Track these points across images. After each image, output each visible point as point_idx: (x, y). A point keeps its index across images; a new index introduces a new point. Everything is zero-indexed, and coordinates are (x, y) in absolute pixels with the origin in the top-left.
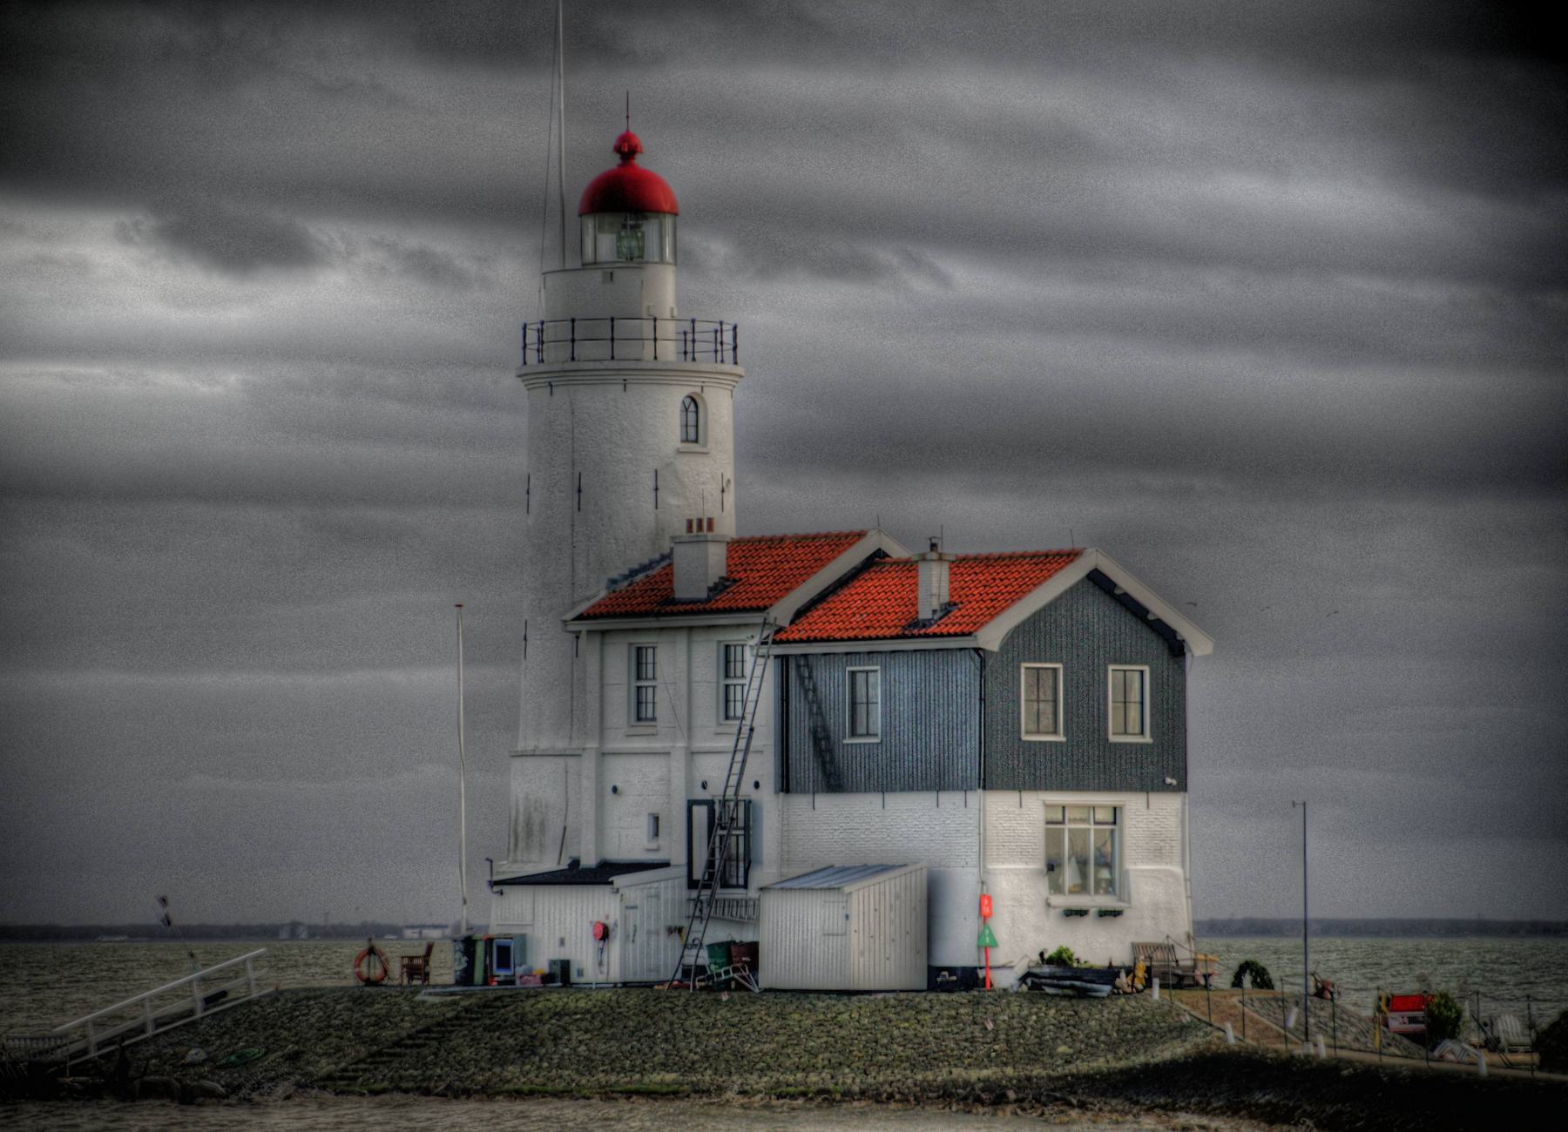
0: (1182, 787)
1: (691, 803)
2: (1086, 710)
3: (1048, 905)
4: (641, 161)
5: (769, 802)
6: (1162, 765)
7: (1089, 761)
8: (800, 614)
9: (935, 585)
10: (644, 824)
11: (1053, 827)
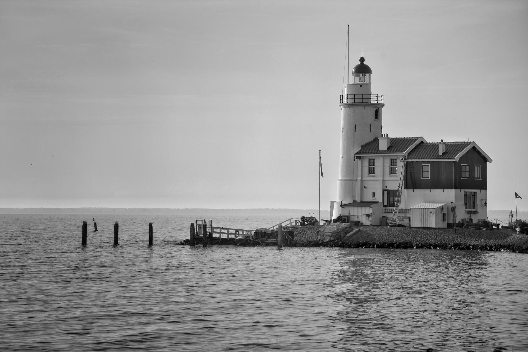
1: (384, 191)
4: (365, 63)
8: (410, 153)
11: (466, 194)
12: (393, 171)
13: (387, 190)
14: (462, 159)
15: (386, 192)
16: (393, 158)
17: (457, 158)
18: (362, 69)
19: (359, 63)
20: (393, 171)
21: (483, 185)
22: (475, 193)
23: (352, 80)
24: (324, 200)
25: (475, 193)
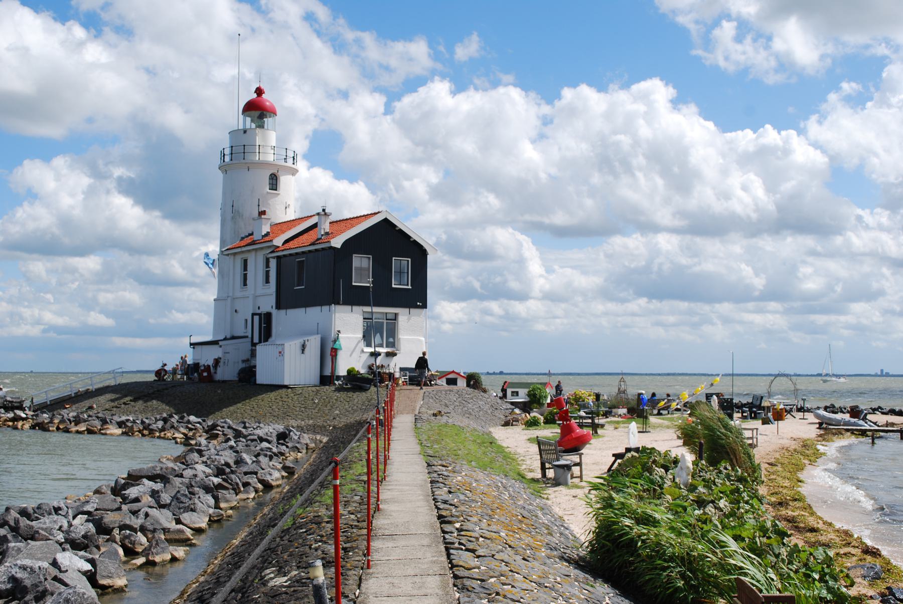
1: (253, 315)
3: (363, 351)
5: (274, 312)
7: (382, 294)
9: (326, 227)
10: (243, 322)
12: (267, 281)
13: (260, 315)
14: (347, 243)
15: (256, 318)
16: (244, 256)
17: (337, 242)
18: (257, 109)
19: (255, 96)
21: (416, 298)
22: (396, 315)
23: (236, 119)
25: (396, 315)
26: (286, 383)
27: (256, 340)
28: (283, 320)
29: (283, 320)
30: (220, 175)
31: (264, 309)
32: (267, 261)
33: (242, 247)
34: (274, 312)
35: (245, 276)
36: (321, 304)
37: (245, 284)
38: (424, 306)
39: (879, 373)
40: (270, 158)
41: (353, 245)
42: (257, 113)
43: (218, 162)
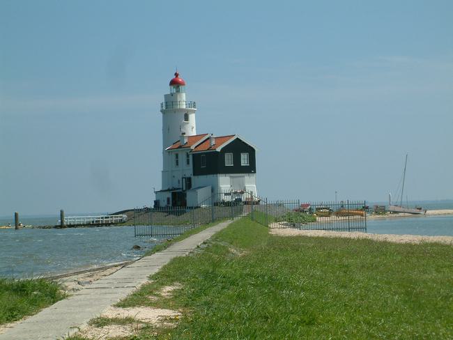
0: (255, 172)
1: (183, 178)
2: (237, 160)
5: (192, 176)
6: (251, 169)
7: (237, 169)
12: (188, 163)
14: (222, 150)
15: (184, 179)
17: (219, 149)
18: (175, 83)
19: (175, 77)
20: (188, 163)
21: (251, 169)
24: (160, 188)
26: (60, 214)
27: (184, 189)
28: (197, 181)
29: (197, 181)
30: (161, 115)
31: (188, 176)
32: (188, 156)
33: (176, 149)
34: (192, 176)
35: (177, 162)
36: (213, 174)
37: (177, 164)
38: (255, 172)
39: (151, 205)
40: (184, 107)
41: (225, 150)
42: (176, 86)
43: (160, 109)
